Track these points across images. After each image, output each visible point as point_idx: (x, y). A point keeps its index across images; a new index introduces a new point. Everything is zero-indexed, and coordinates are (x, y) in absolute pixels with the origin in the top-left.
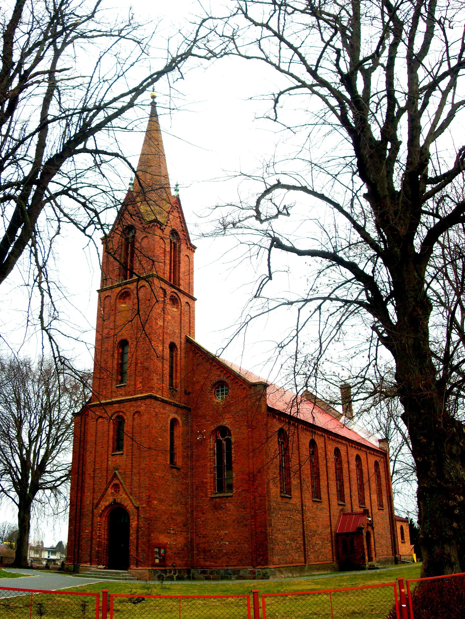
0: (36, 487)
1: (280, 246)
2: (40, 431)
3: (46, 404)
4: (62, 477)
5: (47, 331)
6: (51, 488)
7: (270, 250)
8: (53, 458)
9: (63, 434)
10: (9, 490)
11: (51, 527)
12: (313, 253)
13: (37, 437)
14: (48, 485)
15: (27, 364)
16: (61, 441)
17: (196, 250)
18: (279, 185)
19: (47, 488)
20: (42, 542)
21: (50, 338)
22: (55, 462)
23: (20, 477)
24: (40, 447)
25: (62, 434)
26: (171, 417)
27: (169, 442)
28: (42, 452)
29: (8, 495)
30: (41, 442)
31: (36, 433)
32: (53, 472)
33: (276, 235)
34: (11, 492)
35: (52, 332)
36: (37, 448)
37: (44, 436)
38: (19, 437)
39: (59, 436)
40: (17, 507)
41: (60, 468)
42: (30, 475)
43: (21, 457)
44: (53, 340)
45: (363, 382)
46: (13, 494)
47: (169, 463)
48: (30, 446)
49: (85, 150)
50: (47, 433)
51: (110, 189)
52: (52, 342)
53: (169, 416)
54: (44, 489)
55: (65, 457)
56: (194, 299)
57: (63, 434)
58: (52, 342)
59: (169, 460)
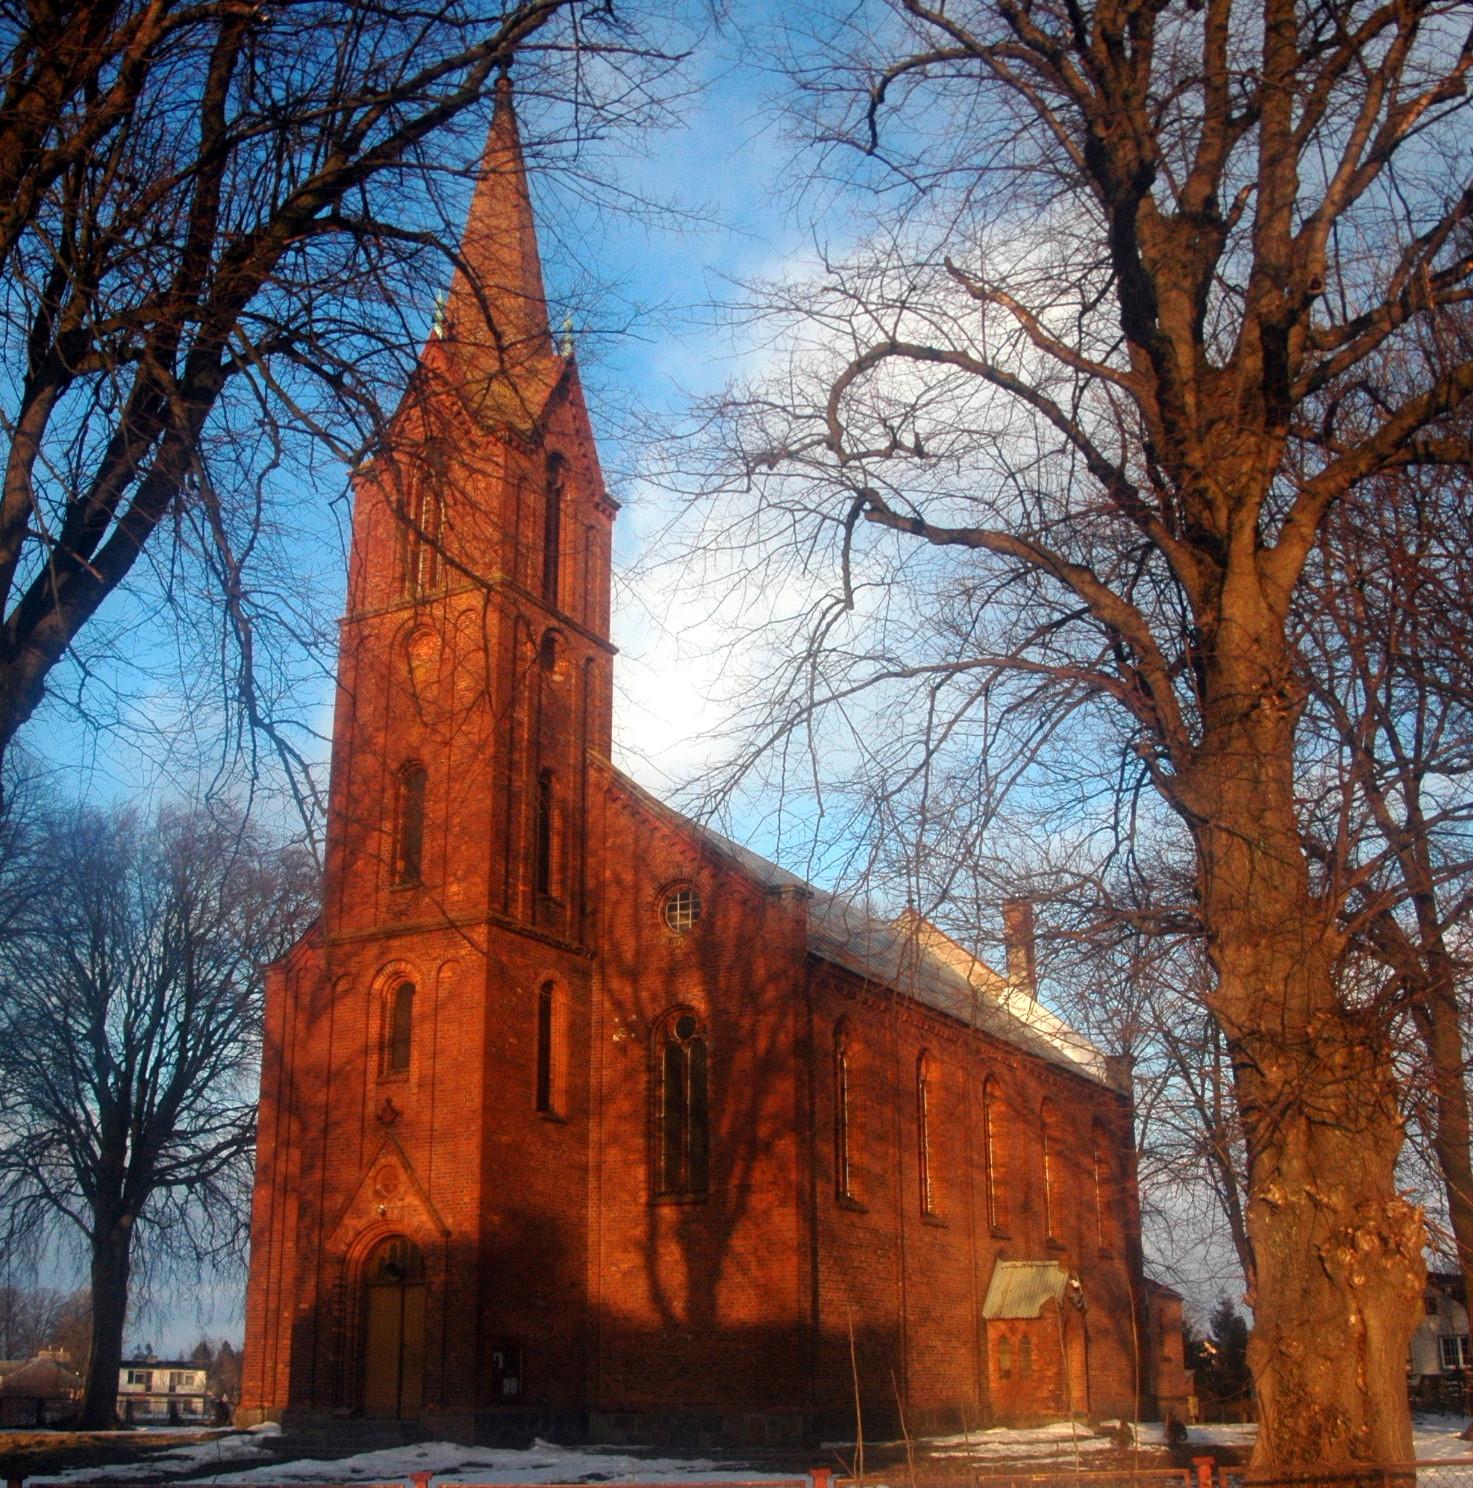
0: (145, 1177)
1: (881, 513)
2: (159, 1013)
3: (178, 934)
4: (220, 1147)
5: (269, 729)
6: (189, 1182)
7: (849, 525)
8: (198, 1093)
9: (225, 1024)
10: (67, 1191)
11: (197, 1308)
12: (967, 538)
13: (149, 1034)
14: (182, 1173)
15: (127, 822)
16: (218, 1043)
17: (619, 514)
18: (894, 348)
19: (178, 1182)
20: (149, 1347)
21: (282, 747)
22: (200, 1105)
23: (98, 1152)
24: (159, 1062)
25: (220, 1025)
26: (542, 979)
27: (535, 1048)
28: (165, 1077)
29: (61, 1208)
30: (162, 1044)
31: (147, 1021)
32: (195, 1133)
33: (873, 483)
34: (74, 1199)
35: (281, 730)
36: (151, 1064)
37: (170, 1028)
38: (97, 1036)
39: (216, 1030)
40: (86, 1242)
41: (216, 1122)
42: (128, 1142)
43: (101, 1093)
44: (291, 751)
45: (1081, 886)
46: (77, 1202)
47: (534, 1106)
48: (130, 1059)
49: (338, 222)
50: (181, 1019)
51: (404, 340)
52: (288, 756)
53: (537, 974)
54: (169, 1184)
55: (238, 1090)
56: (613, 650)
57: (225, 1024)
58: (288, 756)
59: (534, 1099)
